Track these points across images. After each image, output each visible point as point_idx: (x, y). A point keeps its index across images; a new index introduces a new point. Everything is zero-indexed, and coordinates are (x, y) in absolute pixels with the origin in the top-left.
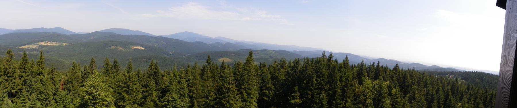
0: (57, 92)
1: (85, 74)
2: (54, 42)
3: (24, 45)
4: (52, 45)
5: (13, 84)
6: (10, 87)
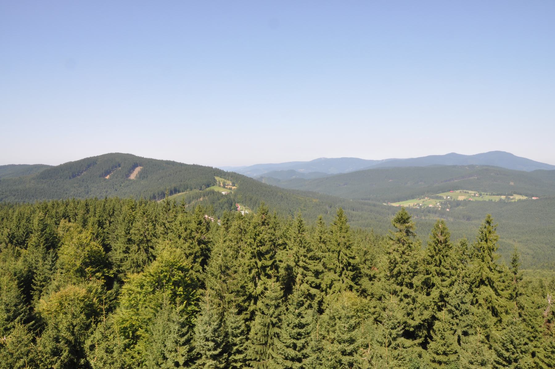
3: (406, 199)
4: (480, 199)
5: (411, 306)
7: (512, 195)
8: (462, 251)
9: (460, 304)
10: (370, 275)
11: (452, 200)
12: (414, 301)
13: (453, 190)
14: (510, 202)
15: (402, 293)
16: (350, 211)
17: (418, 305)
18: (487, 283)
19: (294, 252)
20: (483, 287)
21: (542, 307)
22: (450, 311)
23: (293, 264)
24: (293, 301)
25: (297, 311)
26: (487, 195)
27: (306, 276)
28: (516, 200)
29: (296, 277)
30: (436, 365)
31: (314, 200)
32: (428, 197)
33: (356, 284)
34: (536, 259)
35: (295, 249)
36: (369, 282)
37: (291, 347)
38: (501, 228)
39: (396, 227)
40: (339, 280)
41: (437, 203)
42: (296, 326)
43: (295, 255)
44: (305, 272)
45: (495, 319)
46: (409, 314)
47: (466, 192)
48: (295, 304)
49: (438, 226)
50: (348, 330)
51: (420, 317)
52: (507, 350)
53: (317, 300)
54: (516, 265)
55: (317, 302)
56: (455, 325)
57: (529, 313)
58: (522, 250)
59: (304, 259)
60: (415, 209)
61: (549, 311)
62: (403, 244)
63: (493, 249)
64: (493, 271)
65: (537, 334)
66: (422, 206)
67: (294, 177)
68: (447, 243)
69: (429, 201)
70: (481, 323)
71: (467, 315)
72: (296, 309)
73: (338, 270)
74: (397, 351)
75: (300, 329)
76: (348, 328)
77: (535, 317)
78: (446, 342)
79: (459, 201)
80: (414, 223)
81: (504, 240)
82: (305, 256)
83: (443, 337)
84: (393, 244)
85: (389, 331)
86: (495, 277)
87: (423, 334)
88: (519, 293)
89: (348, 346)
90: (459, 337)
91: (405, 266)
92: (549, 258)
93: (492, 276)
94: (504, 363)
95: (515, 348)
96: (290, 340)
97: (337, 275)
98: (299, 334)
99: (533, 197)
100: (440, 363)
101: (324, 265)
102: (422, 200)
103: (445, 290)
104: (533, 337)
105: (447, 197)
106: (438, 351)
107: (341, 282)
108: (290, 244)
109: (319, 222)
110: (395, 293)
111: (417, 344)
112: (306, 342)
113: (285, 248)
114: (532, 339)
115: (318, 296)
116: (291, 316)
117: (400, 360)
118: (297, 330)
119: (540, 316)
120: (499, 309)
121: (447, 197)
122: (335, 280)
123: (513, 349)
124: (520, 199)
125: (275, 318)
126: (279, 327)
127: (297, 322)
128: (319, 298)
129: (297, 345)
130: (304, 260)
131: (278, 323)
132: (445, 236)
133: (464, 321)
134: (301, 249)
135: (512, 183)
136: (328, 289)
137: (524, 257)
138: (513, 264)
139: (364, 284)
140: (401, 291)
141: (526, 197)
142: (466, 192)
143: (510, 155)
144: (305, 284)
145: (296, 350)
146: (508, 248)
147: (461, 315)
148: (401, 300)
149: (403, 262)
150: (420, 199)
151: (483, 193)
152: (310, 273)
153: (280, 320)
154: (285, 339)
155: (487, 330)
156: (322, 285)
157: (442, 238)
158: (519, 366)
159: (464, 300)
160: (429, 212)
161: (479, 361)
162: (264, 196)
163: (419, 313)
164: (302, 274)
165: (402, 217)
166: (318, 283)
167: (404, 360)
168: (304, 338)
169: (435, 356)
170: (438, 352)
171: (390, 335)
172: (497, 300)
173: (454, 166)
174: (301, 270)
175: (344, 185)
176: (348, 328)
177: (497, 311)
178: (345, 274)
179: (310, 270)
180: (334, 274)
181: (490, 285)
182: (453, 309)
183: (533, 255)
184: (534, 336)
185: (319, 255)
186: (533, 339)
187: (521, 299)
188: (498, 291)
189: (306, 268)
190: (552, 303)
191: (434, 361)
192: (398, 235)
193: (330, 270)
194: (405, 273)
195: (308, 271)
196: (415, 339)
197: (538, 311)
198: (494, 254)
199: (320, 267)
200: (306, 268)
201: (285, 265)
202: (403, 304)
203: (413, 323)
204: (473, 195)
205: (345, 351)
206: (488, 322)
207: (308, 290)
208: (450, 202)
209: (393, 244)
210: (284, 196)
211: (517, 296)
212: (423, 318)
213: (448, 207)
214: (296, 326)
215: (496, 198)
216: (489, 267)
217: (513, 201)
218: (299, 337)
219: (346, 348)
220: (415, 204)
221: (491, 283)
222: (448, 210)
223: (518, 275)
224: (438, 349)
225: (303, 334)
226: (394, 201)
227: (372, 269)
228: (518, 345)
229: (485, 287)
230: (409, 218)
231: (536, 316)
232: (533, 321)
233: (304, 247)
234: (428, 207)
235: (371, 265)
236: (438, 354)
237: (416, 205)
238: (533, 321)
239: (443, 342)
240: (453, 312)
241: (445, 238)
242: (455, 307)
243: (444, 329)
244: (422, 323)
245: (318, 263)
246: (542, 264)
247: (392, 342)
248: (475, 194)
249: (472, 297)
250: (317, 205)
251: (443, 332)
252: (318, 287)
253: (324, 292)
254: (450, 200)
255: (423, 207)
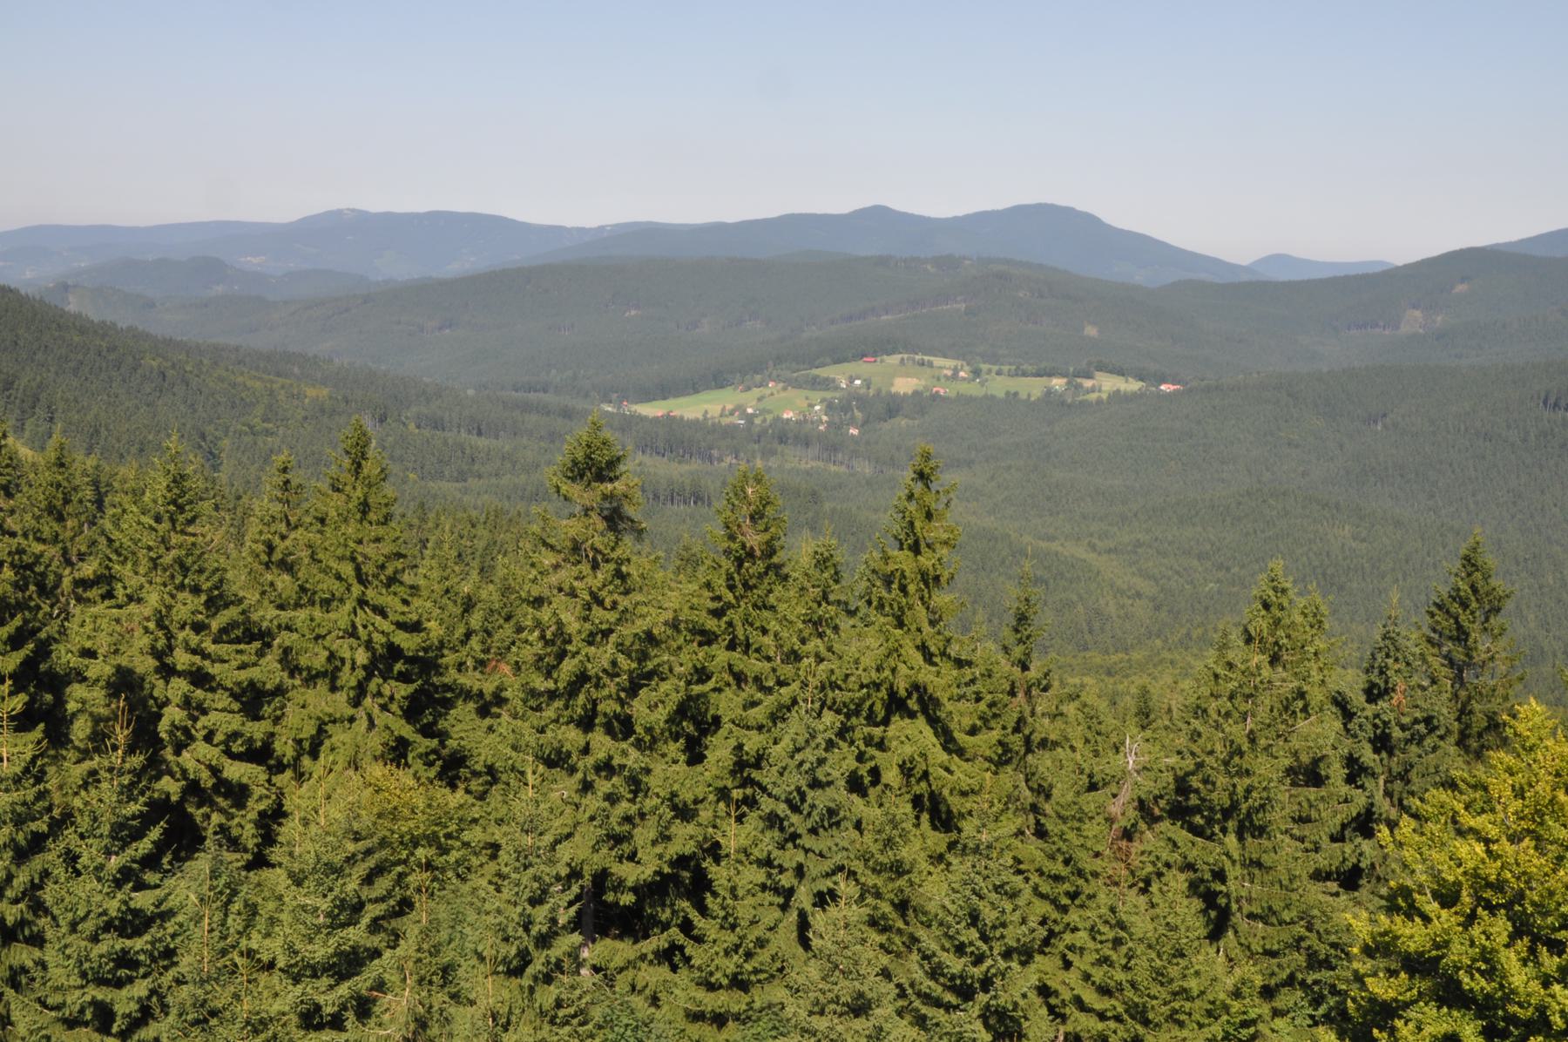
0: (1064, 910)
1: (1382, 743)
2: (993, 358)
3: (691, 387)
4: (974, 389)
5: (624, 807)
6: (591, 833)
7: (1089, 376)
8: (817, 590)
9: (804, 788)
10: (481, 694)
11: (872, 392)
12: (636, 785)
13: (875, 354)
14: (1081, 402)
15: (590, 761)
16: (464, 434)
17: (649, 803)
18: (916, 707)
19: (147, 612)
20: (899, 725)
21: (1105, 784)
22: (773, 820)
23: (144, 665)
24: (95, 819)
25: (115, 862)
26: (999, 373)
27: (205, 712)
28: (1104, 396)
29: (159, 716)
30: (705, 1030)
31: (311, 392)
32: (778, 379)
33: (427, 731)
34: (1163, 615)
35: (153, 599)
36: (478, 721)
37: (86, 1024)
38: (1049, 499)
39: (566, 498)
40: (352, 720)
41: (811, 406)
42: (107, 927)
43: (152, 625)
44: (199, 694)
45: (938, 841)
46: (617, 839)
47: (922, 364)
48: (105, 829)
49: (740, 493)
50: (329, 921)
51: (659, 849)
52: (960, 949)
53: (255, 807)
54: (1028, 637)
55: (253, 815)
56: (790, 874)
57: (1059, 809)
58: (1119, 582)
59: (194, 639)
60: (728, 426)
61: (1128, 798)
62: (595, 566)
63: (937, 578)
64: (937, 660)
65: (1080, 882)
66: (754, 416)
67: (219, 289)
68: (775, 560)
69: (783, 394)
70: (882, 859)
71: (834, 831)
72: (108, 853)
73: (348, 678)
74: (552, 988)
75: (129, 937)
76: (329, 915)
77: (1077, 824)
78: (742, 938)
79: (895, 397)
80: (636, 480)
81: (1055, 546)
82: (198, 628)
83: (731, 920)
84: (556, 567)
85: (519, 909)
86: (941, 682)
87: (674, 912)
88: (1036, 738)
89: (331, 987)
90: (802, 915)
91: (604, 655)
92: (1207, 608)
93: (931, 677)
94: (949, 997)
95: (984, 938)
96: (78, 993)
97: (341, 698)
98: (125, 960)
99: (1164, 381)
100: (719, 1020)
101: (287, 660)
102: (756, 392)
103: (753, 742)
104: (1067, 894)
105: (851, 379)
106: (711, 974)
107: (362, 724)
108: (129, 577)
109: (279, 480)
110: (556, 760)
111: (651, 957)
112: (153, 992)
113: (109, 595)
114: (1065, 901)
115: (258, 791)
116: (87, 887)
117: (567, 1023)
118: (112, 943)
119: (1100, 819)
120: (956, 803)
121: (851, 379)
122: (334, 722)
123: (980, 943)
124: (1118, 391)
125: (16, 901)
126: (38, 941)
127: (113, 906)
128: (261, 798)
129: (116, 1007)
130: (193, 644)
131: (30, 923)
132: (766, 530)
133: (821, 855)
134: (180, 596)
135: (1091, 331)
136: (306, 761)
137: (1123, 607)
138: (1017, 631)
139: (456, 732)
140: (586, 750)
141: (1140, 384)
142: (922, 364)
143: (1091, 220)
144: (202, 749)
145: (109, 1033)
146: (1068, 575)
147: (813, 831)
148: (587, 787)
149: (592, 634)
150: (748, 389)
151: (984, 367)
152: (222, 700)
153: (39, 907)
154: (57, 989)
155: (902, 882)
156: (278, 746)
157: (754, 540)
158: (993, 1002)
159: (820, 775)
160: (782, 439)
161: (843, 1000)
162: (76, 371)
163: (652, 834)
164: (186, 703)
165: (588, 457)
166: (258, 736)
167: (582, 1024)
168: (145, 976)
169: (701, 994)
170: (713, 980)
171: (527, 929)
172: (947, 770)
173: (883, 261)
174: (179, 687)
175: (440, 329)
176: (329, 915)
177: (949, 812)
178: (379, 694)
179: (220, 685)
180: (330, 697)
181: (925, 711)
182: (782, 809)
183: (1153, 599)
184: (1072, 889)
185: (263, 618)
186: (1069, 902)
187: (1042, 762)
188: (956, 734)
189: (200, 679)
190: (1140, 767)
191: (696, 1017)
192: (571, 528)
193: (311, 679)
194: (599, 679)
195: (213, 690)
196: (646, 937)
197: (1090, 801)
198: (940, 599)
199: (268, 671)
200: (200, 679)
201: (108, 670)
202: (593, 803)
203: (631, 874)
204: (949, 373)
205: (318, 1008)
206: (905, 853)
207: (215, 771)
208: (862, 401)
209: (556, 567)
210: (170, 373)
211: (1029, 750)
212: (674, 849)
213: (852, 422)
214: (107, 927)
215: (1033, 388)
216: (923, 648)
217: (1093, 397)
218: (122, 973)
219: (321, 999)
220: (729, 407)
221: (928, 707)
222: (854, 431)
223: (1034, 673)
224: (712, 968)
225: (142, 957)
226: (647, 396)
227: (488, 670)
228: (994, 927)
229: (907, 721)
230: (619, 459)
231: (1080, 820)
232: (1071, 836)
233: (196, 590)
234: (778, 419)
235: (486, 651)
236: (712, 987)
237: (732, 413)
238: (1071, 836)
239: (730, 938)
240: (782, 820)
241: (767, 536)
242: (788, 802)
243: (733, 890)
244: (667, 870)
245: (260, 654)
246: (1184, 631)
247: (535, 954)
248: (956, 371)
249: (851, 763)
250: (323, 411)
251: (729, 901)
252: (260, 754)
253: (289, 774)
254: (863, 391)
255: (757, 421)
